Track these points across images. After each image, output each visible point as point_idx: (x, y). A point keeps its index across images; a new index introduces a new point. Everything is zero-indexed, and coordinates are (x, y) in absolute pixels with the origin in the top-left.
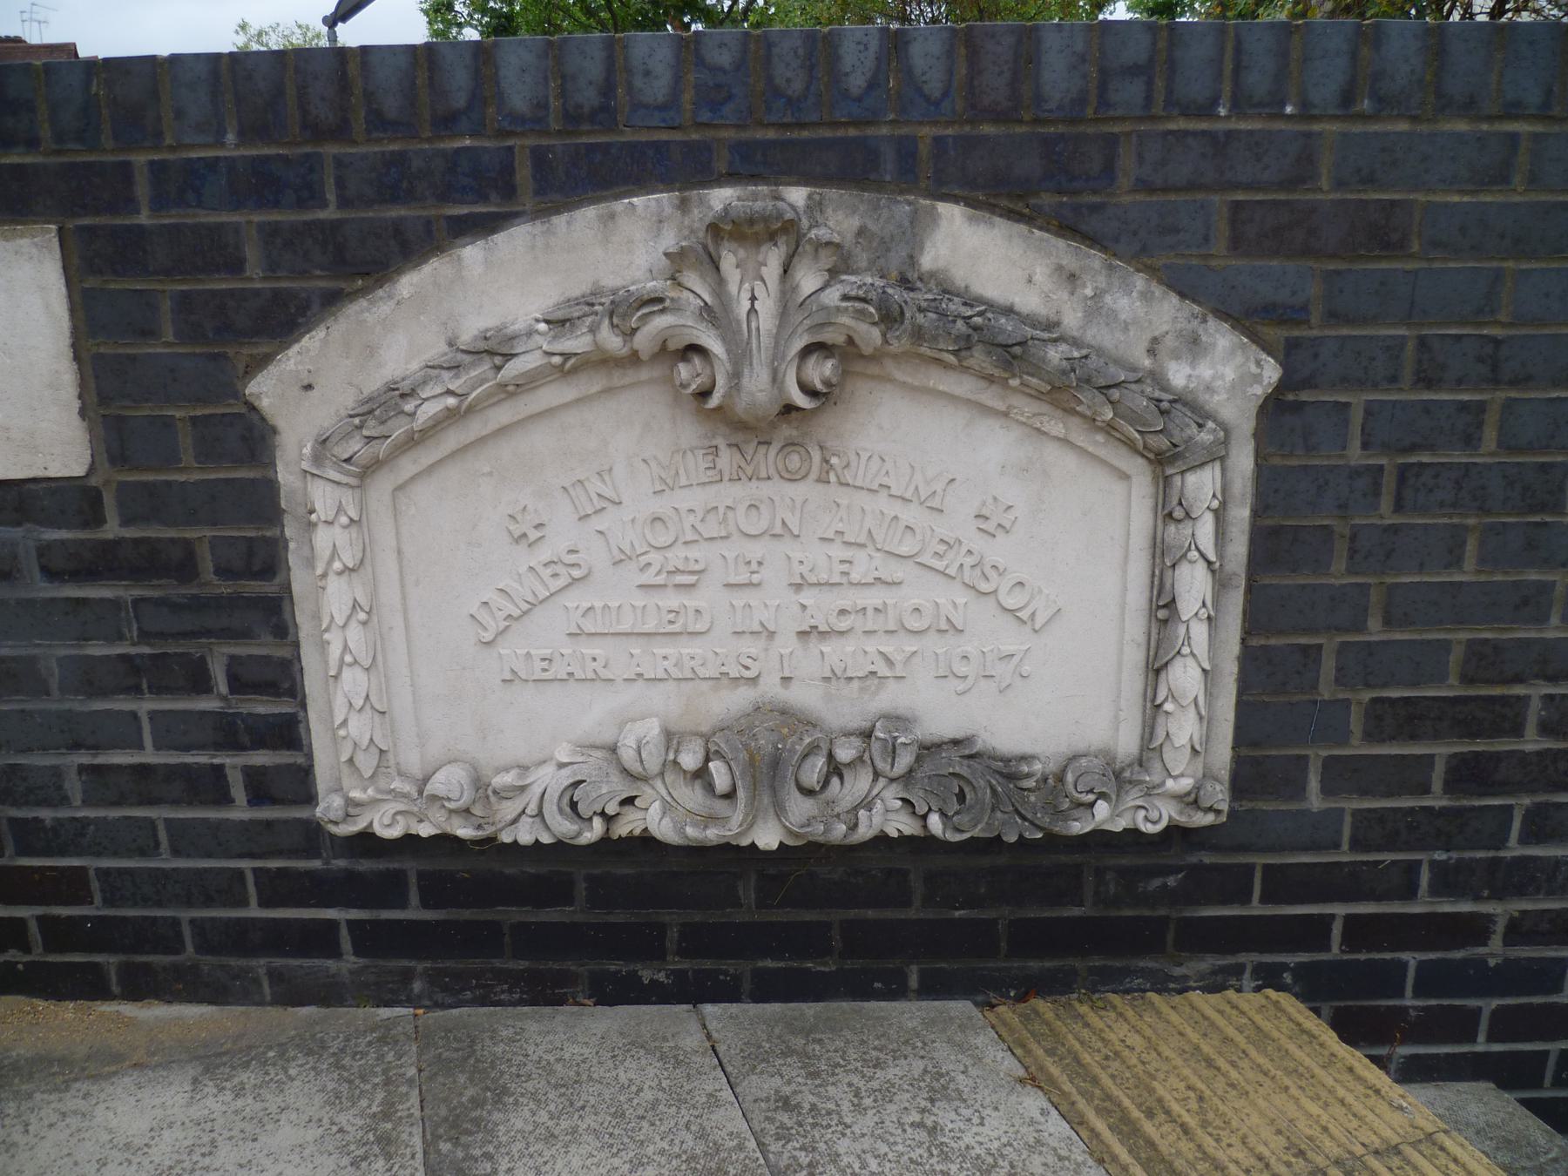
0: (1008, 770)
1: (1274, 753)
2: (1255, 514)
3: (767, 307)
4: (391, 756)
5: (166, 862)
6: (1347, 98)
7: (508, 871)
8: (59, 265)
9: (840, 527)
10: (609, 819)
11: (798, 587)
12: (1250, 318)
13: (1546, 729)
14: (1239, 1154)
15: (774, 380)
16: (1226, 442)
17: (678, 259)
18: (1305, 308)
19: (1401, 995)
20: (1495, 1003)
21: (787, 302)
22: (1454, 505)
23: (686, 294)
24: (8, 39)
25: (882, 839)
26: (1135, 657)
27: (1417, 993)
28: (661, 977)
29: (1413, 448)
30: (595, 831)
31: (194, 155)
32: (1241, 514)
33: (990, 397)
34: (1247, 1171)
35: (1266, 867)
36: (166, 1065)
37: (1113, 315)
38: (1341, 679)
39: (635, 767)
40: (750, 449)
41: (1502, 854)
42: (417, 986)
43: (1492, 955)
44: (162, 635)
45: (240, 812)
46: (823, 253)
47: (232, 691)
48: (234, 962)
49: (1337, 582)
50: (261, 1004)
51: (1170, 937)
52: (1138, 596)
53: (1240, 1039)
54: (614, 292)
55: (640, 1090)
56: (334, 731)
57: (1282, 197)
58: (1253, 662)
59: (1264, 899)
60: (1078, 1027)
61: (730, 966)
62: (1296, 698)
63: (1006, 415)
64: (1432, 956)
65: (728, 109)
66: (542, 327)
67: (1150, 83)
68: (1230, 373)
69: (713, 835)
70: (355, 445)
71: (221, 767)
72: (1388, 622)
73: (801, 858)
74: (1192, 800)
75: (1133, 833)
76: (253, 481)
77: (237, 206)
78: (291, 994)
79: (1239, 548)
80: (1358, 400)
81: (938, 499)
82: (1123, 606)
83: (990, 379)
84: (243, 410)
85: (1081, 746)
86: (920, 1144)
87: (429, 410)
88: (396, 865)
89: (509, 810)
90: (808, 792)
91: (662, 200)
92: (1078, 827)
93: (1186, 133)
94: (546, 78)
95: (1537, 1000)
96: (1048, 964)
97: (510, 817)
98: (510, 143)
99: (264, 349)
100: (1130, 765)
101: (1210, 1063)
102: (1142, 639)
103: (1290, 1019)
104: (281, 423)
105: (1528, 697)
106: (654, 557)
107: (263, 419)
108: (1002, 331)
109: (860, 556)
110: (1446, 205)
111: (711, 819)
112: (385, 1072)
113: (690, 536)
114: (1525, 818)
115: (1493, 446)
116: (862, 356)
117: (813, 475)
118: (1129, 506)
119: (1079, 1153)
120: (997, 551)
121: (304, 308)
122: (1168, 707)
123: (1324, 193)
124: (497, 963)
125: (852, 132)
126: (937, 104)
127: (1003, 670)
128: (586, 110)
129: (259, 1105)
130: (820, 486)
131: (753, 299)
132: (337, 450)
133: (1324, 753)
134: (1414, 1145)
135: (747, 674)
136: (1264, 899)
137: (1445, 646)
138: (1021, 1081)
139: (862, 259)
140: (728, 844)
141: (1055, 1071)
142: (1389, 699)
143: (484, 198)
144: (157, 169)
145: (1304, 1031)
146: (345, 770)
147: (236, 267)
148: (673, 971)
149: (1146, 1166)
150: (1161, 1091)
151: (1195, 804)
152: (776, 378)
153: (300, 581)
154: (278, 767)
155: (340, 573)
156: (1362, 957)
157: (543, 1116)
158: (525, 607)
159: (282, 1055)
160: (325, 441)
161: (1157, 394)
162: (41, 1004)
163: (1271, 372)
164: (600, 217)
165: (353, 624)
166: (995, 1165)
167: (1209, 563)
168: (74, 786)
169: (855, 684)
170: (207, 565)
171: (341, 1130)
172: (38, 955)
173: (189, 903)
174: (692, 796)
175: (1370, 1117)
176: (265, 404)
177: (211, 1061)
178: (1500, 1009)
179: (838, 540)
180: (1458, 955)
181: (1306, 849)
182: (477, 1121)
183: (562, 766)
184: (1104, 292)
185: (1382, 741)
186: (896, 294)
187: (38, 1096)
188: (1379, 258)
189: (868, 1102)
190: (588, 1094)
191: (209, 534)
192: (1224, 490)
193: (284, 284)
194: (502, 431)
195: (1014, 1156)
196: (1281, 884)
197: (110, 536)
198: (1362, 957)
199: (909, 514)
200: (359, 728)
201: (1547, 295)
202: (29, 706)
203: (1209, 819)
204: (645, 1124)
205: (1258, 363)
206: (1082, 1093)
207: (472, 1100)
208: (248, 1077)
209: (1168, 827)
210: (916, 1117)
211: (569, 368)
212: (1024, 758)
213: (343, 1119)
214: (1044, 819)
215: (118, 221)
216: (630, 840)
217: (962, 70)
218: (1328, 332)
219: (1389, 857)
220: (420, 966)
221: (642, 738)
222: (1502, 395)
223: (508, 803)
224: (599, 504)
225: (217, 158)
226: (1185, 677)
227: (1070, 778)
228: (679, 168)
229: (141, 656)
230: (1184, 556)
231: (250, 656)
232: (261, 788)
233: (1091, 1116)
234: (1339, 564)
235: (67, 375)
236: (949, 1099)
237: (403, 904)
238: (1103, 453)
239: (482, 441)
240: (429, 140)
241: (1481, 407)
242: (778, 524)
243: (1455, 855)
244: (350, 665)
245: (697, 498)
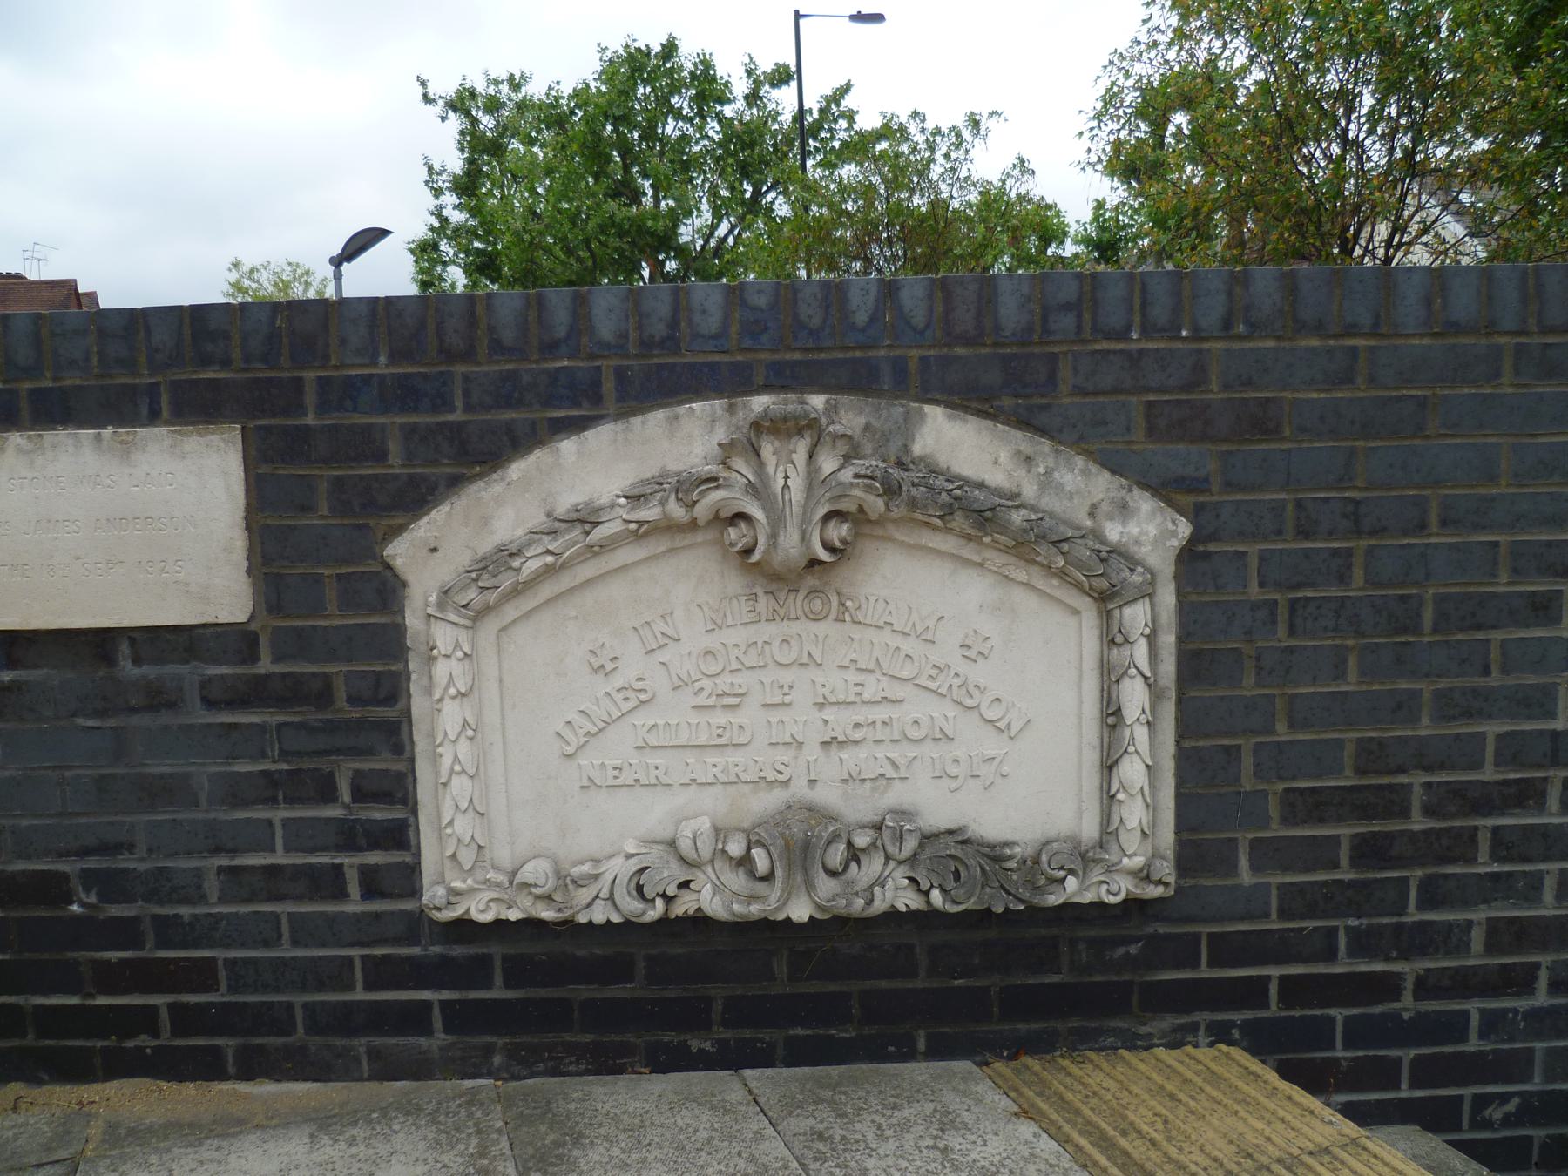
0: (994, 854)
1: (1209, 836)
2: (1180, 640)
3: (797, 484)
4: (486, 851)
5: (287, 952)
6: (1227, 324)
7: (581, 953)
8: (240, 455)
9: (854, 656)
10: (668, 899)
11: (821, 706)
12: (1166, 489)
13: (1428, 811)
14: (1200, 1159)
15: (803, 539)
16: (1153, 582)
17: (728, 449)
18: (1206, 480)
19: (1332, 1047)
20: (1413, 1052)
21: (813, 480)
22: (1335, 630)
23: (734, 474)
24: (9, 276)
25: (892, 915)
26: (1092, 757)
27: (1347, 1045)
28: (707, 1046)
29: (1299, 586)
30: (656, 911)
31: (353, 373)
32: (1168, 640)
33: (968, 551)
34: (1205, 1169)
35: (1210, 935)
36: (286, 1125)
37: (1061, 487)
38: (1258, 773)
39: (689, 853)
40: (782, 596)
41: (1404, 919)
42: (497, 1060)
43: (1407, 1010)
44: (299, 754)
45: (354, 906)
46: (839, 443)
47: (354, 800)
48: (339, 1042)
49: (1249, 694)
50: (361, 1079)
51: (1135, 999)
52: (1091, 708)
53: (1199, 1081)
54: (678, 474)
55: (696, 1131)
56: (440, 830)
57: (1184, 397)
58: (1186, 760)
59: (1211, 964)
60: (1061, 1076)
61: (766, 1034)
62: (1223, 791)
63: (981, 565)
64: (1355, 1011)
65: (765, 338)
66: (623, 501)
67: (1079, 316)
68: (1152, 530)
69: (755, 910)
70: (471, 594)
71: (341, 866)
72: (1292, 726)
74: (1144, 875)
75: (1100, 905)
76: (384, 625)
77: (385, 411)
78: (387, 1069)
79: (1169, 667)
80: (1253, 549)
81: (930, 632)
82: (1080, 716)
83: (968, 538)
84: (379, 568)
85: (1052, 833)
86: (935, 1160)
87: (533, 565)
88: (485, 950)
89: (584, 895)
90: (833, 874)
91: (716, 405)
92: (1053, 899)
93: (1108, 352)
94: (627, 317)
95: (1448, 1049)
96: (1035, 1026)
97: (585, 902)
98: (597, 363)
99: (400, 521)
100: (1093, 848)
101: (1172, 1097)
102: (1096, 742)
103: (1239, 1065)
104: (410, 577)
105: (1410, 785)
106: (706, 683)
107: (396, 576)
108: (976, 500)
109: (870, 680)
110: (1308, 401)
111: (753, 898)
112: (476, 1125)
113: (735, 666)
114: (1419, 888)
115: (1361, 583)
116: (870, 521)
117: (832, 616)
118: (1081, 636)
119: (1066, 1161)
120: (977, 673)
121: (433, 489)
122: (1120, 796)
123: (1215, 393)
124: (568, 1037)
125: (858, 354)
126: (922, 333)
127: (986, 771)
128: (657, 339)
129: (371, 1151)
130: (838, 624)
131: (786, 477)
132: (456, 598)
133: (1250, 836)
134: (1343, 1147)
135: (781, 778)
136: (1211, 964)
137: (1339, 743)
138: (1016, 1114)
139: (868, 448)
140: (766, 919)
141: (1043, 1106)
142: (1298, 789)
143: (578, 405)
144: (323, 383)
145: (1251, 1073)
146: (448, 864)
147: (381, 456)
148: (718, 1041)
149: (1122, 1168)
150: (1132, 1117)
151: (1147, 879)
152: (804, 538)
153: (419, 705)
154: (389, 866)
155: (454, 698)
156: (1297, 1013)
157: (616, 1152)
158: (602, 725)
159: (384, 1116)
160: (446, 592)
161: (1097, 546)
162: (164, 1085)
163: (1184, 529)
164: (668, 418)
165: (463, 739)
166: (998, 1172)
167: (1146, 678)
168: (212, 886)
169: (868, 785)
170: (341, 694)
171: (445, 1166)
172: (165, 1040)
173: (304, 988)
174: (737, 881)
175: (1305, 1129)
176: (398, 563)
177: (323, 1122)
178: (1417, 1058)
179: (853, 667)
180: (1378, 1010)
181: (1242, 919)
182: (560, 1157)
183: (629, 856)
184: (1053, 470)
185: (1295, 825)
186: (895, 473)
187: (176, 1151)
188: (1260, 441)
189: (889, 1133)
190: (653, 1134)
191: (345, 669)
192: (1154, 621)
193: (418, 470)
194: (588, 582)
195: (1013, 1166)
196: (1226, 950)
197: (263, 671)
198: (1297, 1013)
199: (908, 646)
200: (464, 827)
201: (1391, 466)
202: (180, 816)
203: (1158, 891)
204: (703, 1154)
205: (1174, 522)
206: (1068, 1121)
207: (554, 1142)
208: (359, 1132)
209: (1125, 901)
210: (931, 1143)
211: (641, 533)
212: (1006, 844)
213: (445, 1158)
214: (1024, 893)
215: (289, 422)
217: (940, 308)
218: (1225, 498)
219: (1311, 924)
220: (500, 1041)
221: (696, 830)
222: (1364, 543)
223: (584, 890)
224: (662, 640)
225: (372, 375)
226: (1132, 771)
227: (1044, 858)
228: (730, 382)
229: (280, 772)
230: (1125, 673)
231: (371, 770)
232: (373, 884)
233: (1075, 1136)
234: (1249, 679)
235: (239, 541)
236: (957, 1129)
237: (488, 986)
238: (1057, 593)
239: (571, 590)
240: (536, 362)
241: (1349, 553)
242: (805, 654)
243: (1365, 921)
244: (458, 773)
245: (739, 636)
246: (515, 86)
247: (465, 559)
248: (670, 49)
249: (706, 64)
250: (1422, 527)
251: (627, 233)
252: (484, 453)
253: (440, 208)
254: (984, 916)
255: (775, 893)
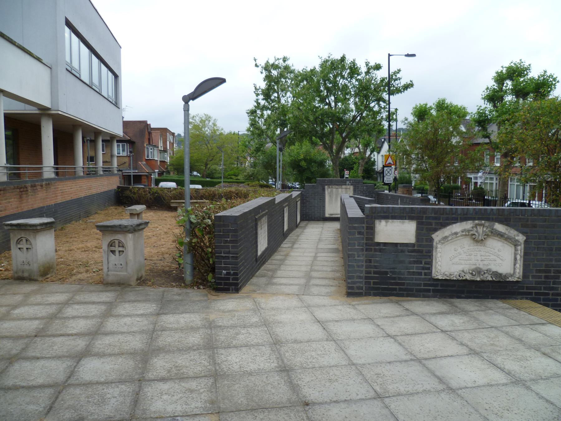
0: (501, 274)
5: (414, 282)
12: (523, 233)
13: (554, 273)
17: (473, 227)
21: (483, 231)
26: (513, 264)
30: (461, 278)
32: (523, 251)
45: (423, 277)
73: (482, 281)
74: (519, 278)
79: (522, 254)
92: (508, 280)
120: (500, 253)
163: (525, 238)
174: (470, 276)
177: (422, 301)
196: (528, 288)
199: (492, 250)
216: (464, 280)
226: (518, 265)
228: (473, 219)
235: (415, 234)
246: (285, 60)
247: (441, 237)
248: (343, 59)
249: (354, 63)
250: (554, 239)
251: (330, 117)
252: (444, 225)
253: (258, 100)
254: (499, 282)
255: (475, 277)
